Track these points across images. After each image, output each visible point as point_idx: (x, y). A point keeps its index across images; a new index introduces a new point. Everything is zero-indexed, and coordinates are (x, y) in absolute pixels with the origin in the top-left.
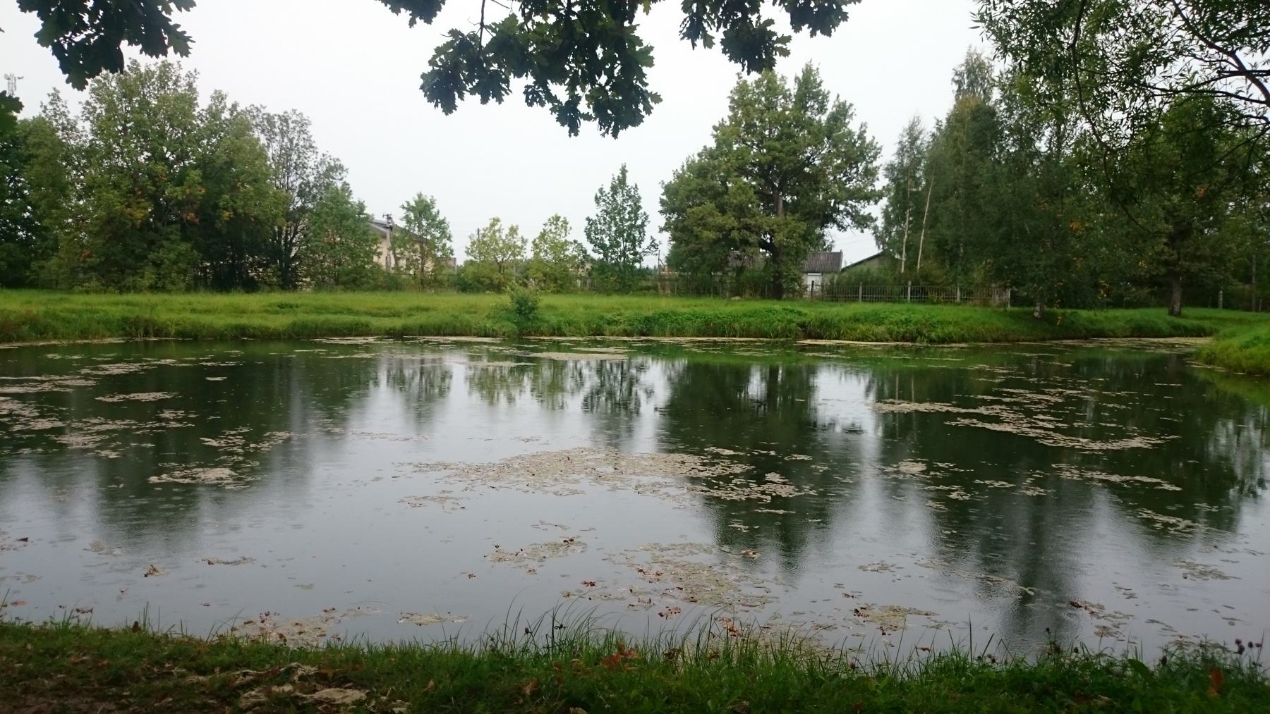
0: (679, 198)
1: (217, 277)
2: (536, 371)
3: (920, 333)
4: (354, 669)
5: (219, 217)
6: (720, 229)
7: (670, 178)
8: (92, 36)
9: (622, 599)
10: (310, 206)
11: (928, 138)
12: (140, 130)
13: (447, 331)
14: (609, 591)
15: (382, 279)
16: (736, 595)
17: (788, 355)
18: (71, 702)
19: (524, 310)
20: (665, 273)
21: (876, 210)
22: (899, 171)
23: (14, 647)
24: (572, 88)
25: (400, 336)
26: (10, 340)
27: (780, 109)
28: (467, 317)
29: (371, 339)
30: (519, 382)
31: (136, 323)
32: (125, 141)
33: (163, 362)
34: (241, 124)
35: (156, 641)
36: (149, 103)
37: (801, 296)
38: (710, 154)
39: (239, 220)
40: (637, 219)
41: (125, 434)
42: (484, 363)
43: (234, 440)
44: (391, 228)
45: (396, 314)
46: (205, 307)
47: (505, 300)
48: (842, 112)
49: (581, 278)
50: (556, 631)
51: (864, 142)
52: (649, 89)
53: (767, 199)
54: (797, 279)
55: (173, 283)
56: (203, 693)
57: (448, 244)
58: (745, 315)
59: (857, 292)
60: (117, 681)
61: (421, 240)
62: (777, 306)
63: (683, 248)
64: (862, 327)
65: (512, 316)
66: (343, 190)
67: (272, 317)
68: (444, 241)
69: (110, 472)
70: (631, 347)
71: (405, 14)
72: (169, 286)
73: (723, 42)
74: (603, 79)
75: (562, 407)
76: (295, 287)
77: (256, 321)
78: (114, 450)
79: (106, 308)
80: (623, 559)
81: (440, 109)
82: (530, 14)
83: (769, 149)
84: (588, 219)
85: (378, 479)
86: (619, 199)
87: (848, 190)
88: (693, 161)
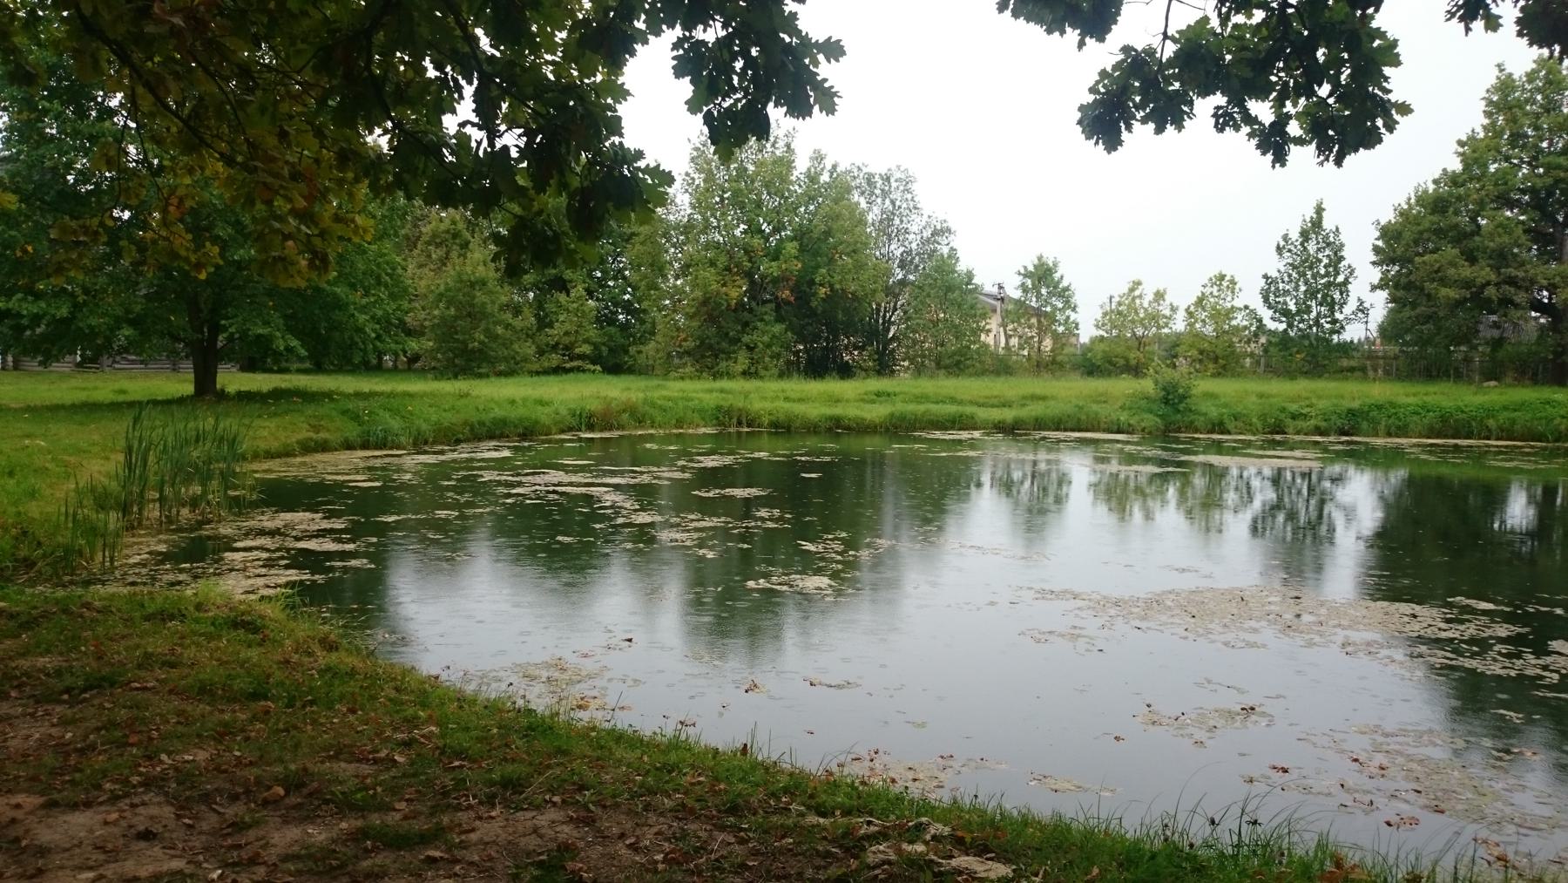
0: (1402, 244)
1: (810, 361)
2: (1186, 480)
4: (995, 837)
5: (815, 294)
6: (1467, 284)
7: (1388, 216)
8: (739, 100)
9: (1329, 794)
10: (912, 277)
12: (738, 201)
13: (1069, 425)
15: (989, 361)
18: (691, 827)
19: (1172, 398)
20: (1378, 347)
23: (631, 756)
24: (1279, 104)
25: (1011, 430)
26: (611, 429)
28: (1095, 407)
29: (977, 434)
30: (1162, 492)
31: (728, 412)
32: (723, 214)
33: (756, 455)
34: (841, 187)
35: (770, 769)
36: (746, 169)
38: (1453, 180)
39: (835, 297)
41: (725, 533)
42: (1114, 467)
43: (829, 546)
44: (1002, 299)
46: (797, 395)
47: (1147, 385)
49: (1252, 355)
52: (1393, 97)
55: (766, 369)
56: (825, 838)
57: (1073, 316)
58: (1505, 408)
60: (734, 810)
61: (1038, 313)
63: (1407, 312)
65: (1155, 407)
66: (950, 257)
67: (868, 406)
68: (1068, 312)
69: (698, 575)
70: (1326, 450)
72: (762, 373)
73: (1519, 21)
74: (1324, 90)
75: (1220, 531)
76: (893, 372)
77: (851, 412)
78: (711, 548)
79: (701, 395)
81: (1101, 146)
82: (1228, 13)
83: (1549, 168)
84: (1266, 277)
85: (992, 603)
86: (1312, 247)
88: (1425, 191)
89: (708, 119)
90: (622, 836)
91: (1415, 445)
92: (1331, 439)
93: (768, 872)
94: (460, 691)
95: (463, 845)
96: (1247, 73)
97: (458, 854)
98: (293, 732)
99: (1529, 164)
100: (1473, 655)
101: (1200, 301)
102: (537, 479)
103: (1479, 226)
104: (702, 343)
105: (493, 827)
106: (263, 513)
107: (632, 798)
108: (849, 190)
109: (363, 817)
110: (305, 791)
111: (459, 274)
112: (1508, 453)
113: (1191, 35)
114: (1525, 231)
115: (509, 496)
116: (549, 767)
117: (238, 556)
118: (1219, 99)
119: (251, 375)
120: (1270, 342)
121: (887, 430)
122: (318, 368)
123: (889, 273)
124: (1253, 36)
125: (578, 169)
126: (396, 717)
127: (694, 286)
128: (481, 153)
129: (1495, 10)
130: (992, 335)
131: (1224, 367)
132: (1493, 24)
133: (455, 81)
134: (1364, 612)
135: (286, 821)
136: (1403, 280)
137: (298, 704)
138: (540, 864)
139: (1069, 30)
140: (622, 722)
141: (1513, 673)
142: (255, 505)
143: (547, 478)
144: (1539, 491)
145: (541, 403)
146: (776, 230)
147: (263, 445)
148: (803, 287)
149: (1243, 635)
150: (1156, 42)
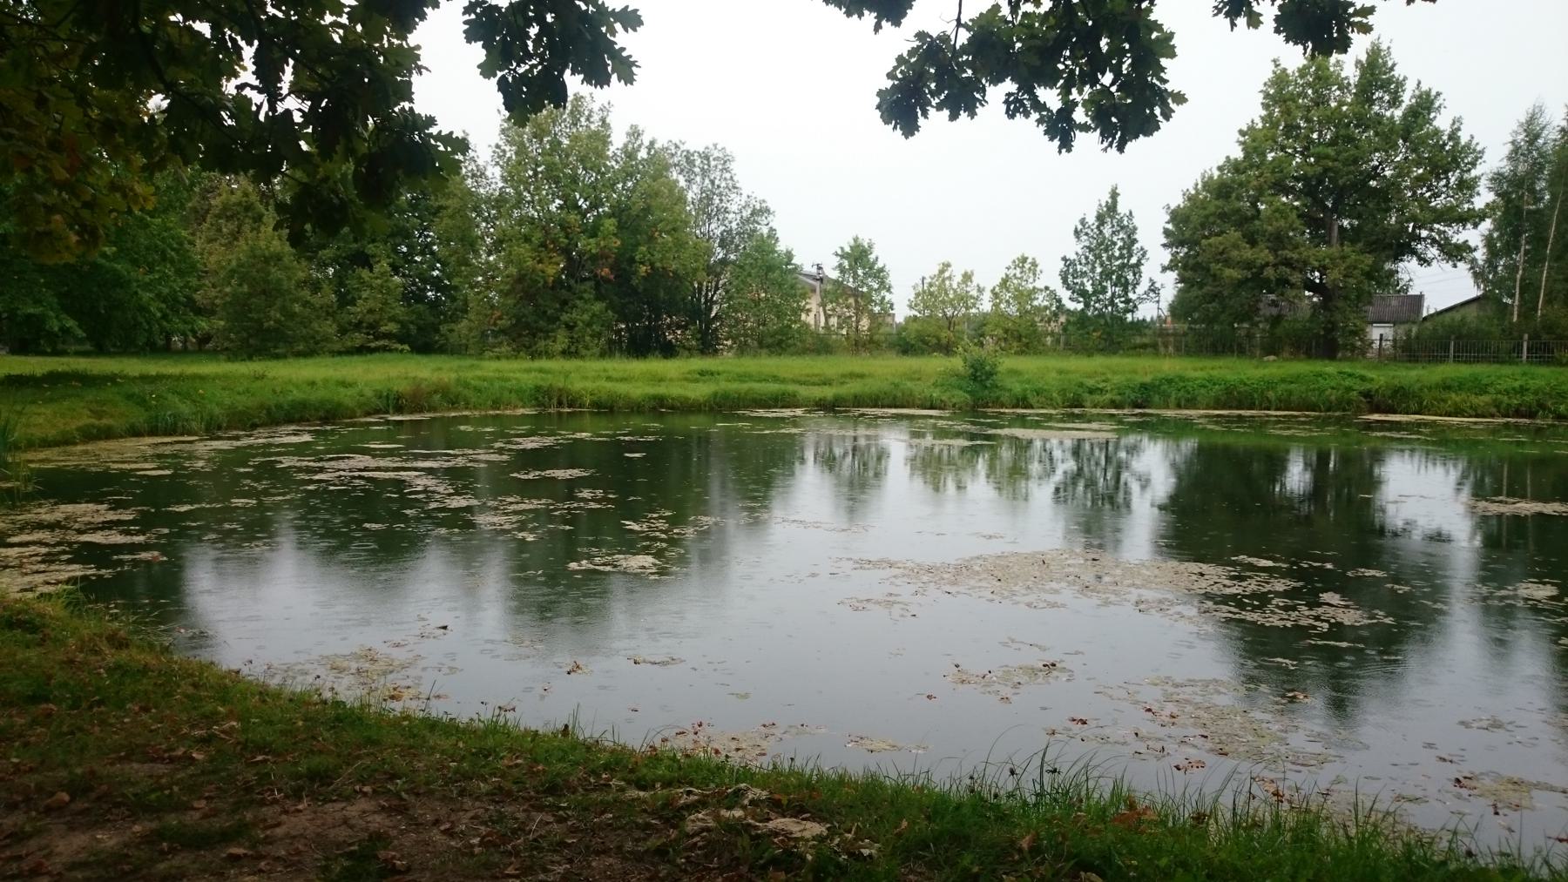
0: (1187, 227)
1: (632, 340)
3: (1542, 406)
6: (1248, 265)
7: (1177, 201)
8: (535, 66)
10: (732, 257)
11: (1555, 135)
12: (552, 176)
13: (886, 402)
14: (1107, 731)
16: (1283, 749)
17: (1345, 434)
18: (508, 809)
19: (980, 375)
21: (1473, 236)
22: (1510, 182)
23: (446, 744)
24: (1066, 91)
25: (831, 407)
26: (421, 411)
27: (1333, 104)
28: (909, 384)
29: (799, 412)
30: (972, 464)
32: (537, 188)
33: (578, 435)
34: (659, 163)
35: (591, 747)
36: (560, 143)
37: (1363, 354)
38: (1235, 167)
39: (656, 275)
40: (1131, 256)
42: (929, 440)
43: (658, 524)
44: (821, 280)
45: (826, 382)
46: (620, 375)
47: (957, 363)
48: (1425, 104)
49: (1052, 334)
50: (1047, 777)
51: (1457, 143)
52: (1169, 87)
53: (1317, 224)
54: (1359, 332)
55: (587, 348)
56: (645, 811)
57: (888, 297)
58: (1283, 381)
59: (1447, 349)
60: (553, 789)
61: (855, 293)
62: (1330, 368)
63: (1195, 292)
64: (1455, 397)
65: (964, 384)
68: (883, 293)
70: (1120, 422)
71: (870, 18)
72: (584, 352)
73: (1277, 19)
74: (1107, 78)
75: (1026, 499)
76: (716, 351)
77: (675, 391)
78: (532, 531)
79: (518, 375)
80: (1123, 694)
81: (899, 132)
83: (1319, 157)
84: (1064, 259)
85: (813, 575)
86: (1107, 231)
87: (1434, 210)
88: (1211, 178)
89: (503, 85)
90: (437, 822)
91: (1201, 417)
92: (1126, 411)
93: (587, 848)
94: (264, 685)
95: (268, 841)
96: (1036, 61)
97: (262, 849)
98: (79, 735)
99: (1302, 153)
100: (1254, 609)
101: (1005, 283)
102: (342, 465)
103: (1258, 211)
104: (518, 320)
105: (301, 820)
106: (40, 506)
107: (446, 784)
108: (667, 167)
109: (159, 818)
110: (93, 795)
111: (252, 249)
112: (1287, 422)
113: (983, 22)
114: (1299, 216)
115: (311, 482)
116: (358, 757)
117: (13, 552)
118: (1009, 86)
119: (23, 358)
120: (1068, 321)
121: (711, 409)
122: (100, 351)
123: (709, 252)
124: (1041, 25)
125: (366, 135)
126: (194, 713)
127: (509, 262)
128: (262, 118)
129: (1256, 8)
130: (812, 315)
131: (1027, 345)
132: (1254, 21)
133: (234, 41)
134: (1157, 572)
135: (72, 828)
136: (1191, 262)
137: (84, 705)
138: (350, 855)
139: (866, 12)
140: (437, 710)
141: (1289, 624)
142: (30, 497)
143: (352, 463)
144: (1315, 458)
145: (344, 384)
146: (594, 206)
147: (38, 433)
148: (623, 264)
149: (1044, 596)
150: (950, 29)
